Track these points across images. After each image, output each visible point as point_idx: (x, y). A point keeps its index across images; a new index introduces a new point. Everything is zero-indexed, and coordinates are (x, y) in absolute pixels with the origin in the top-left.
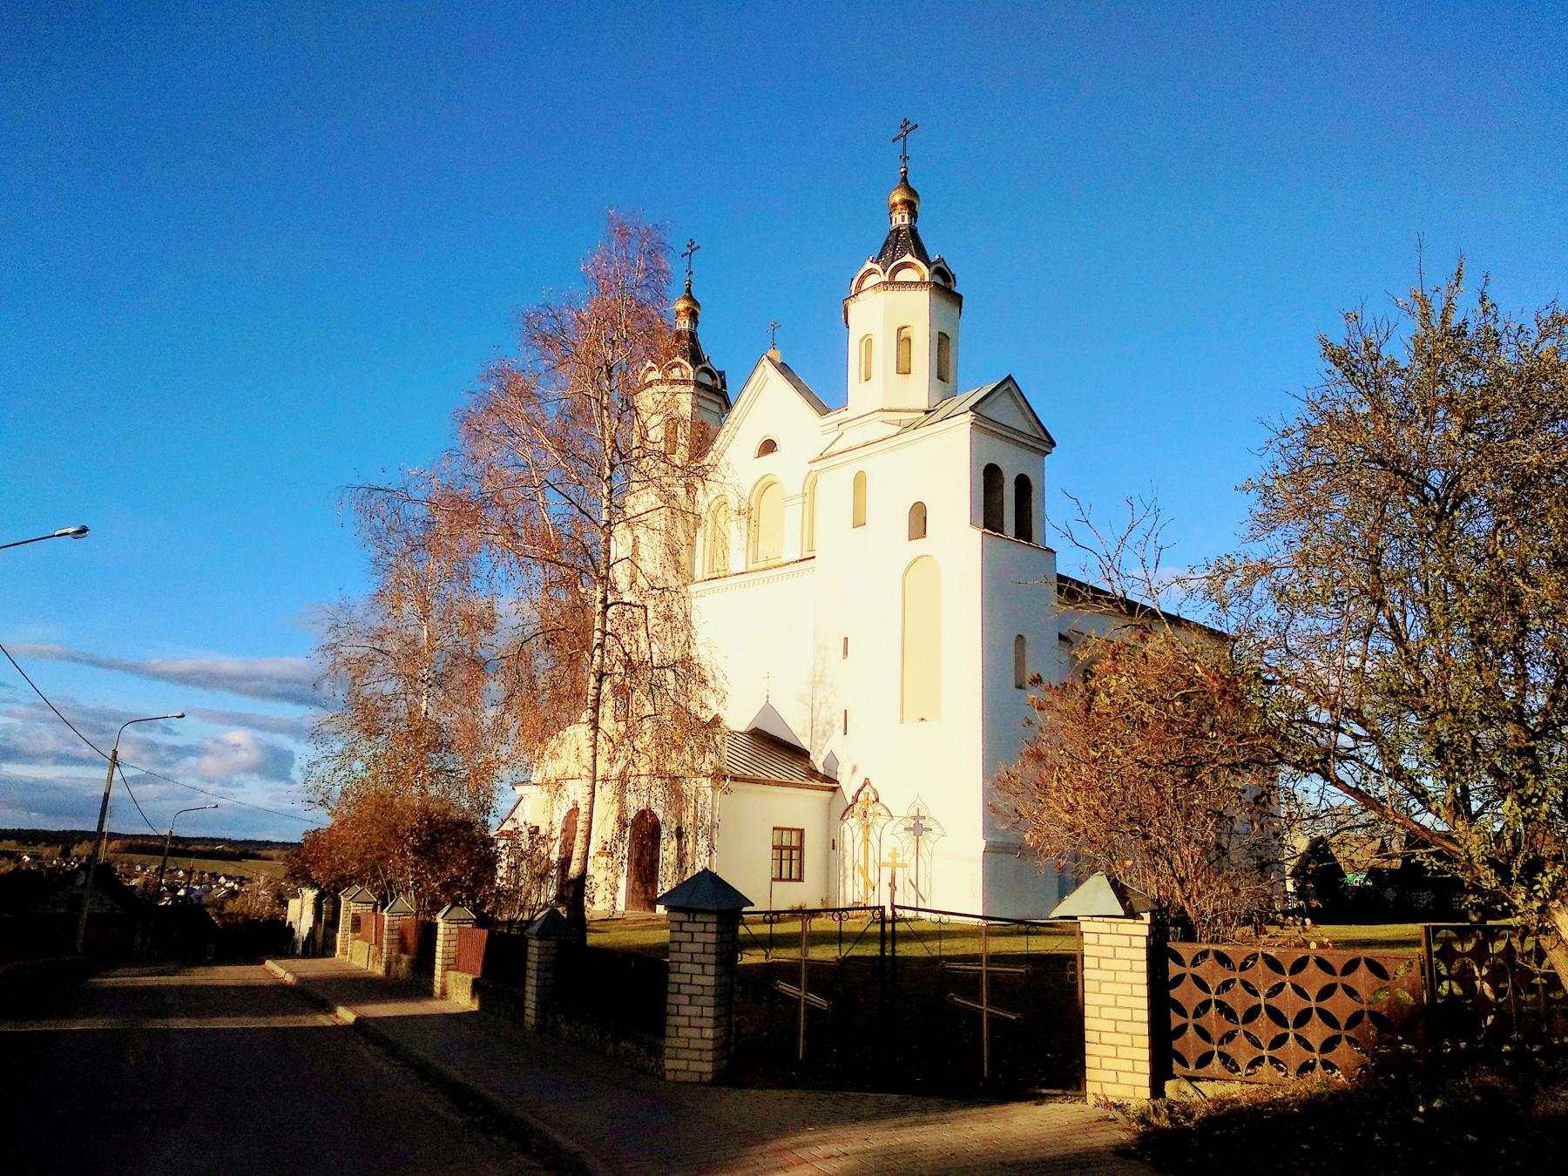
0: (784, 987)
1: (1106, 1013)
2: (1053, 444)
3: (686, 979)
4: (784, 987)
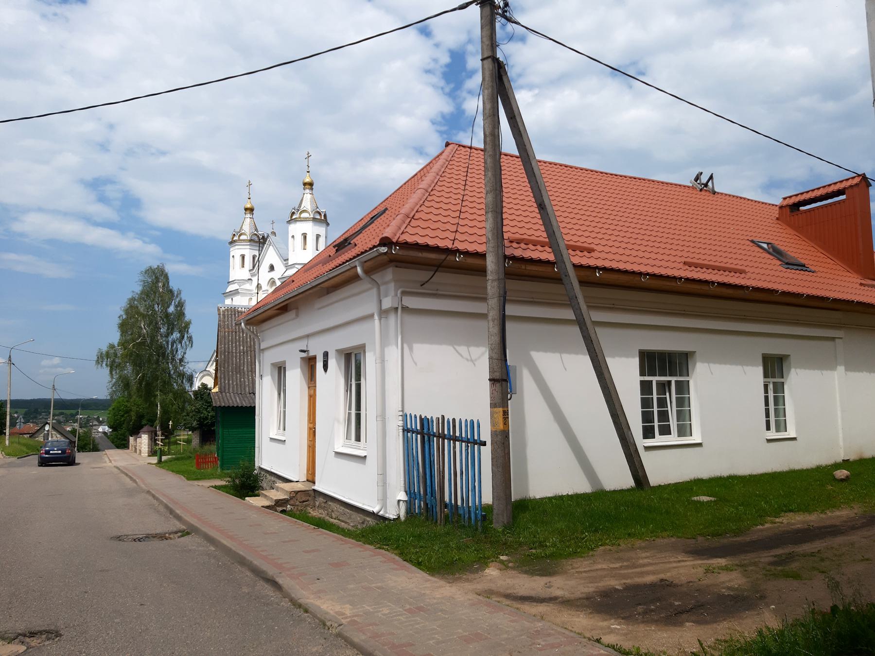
0: (157, 442)
4: (157, 442)
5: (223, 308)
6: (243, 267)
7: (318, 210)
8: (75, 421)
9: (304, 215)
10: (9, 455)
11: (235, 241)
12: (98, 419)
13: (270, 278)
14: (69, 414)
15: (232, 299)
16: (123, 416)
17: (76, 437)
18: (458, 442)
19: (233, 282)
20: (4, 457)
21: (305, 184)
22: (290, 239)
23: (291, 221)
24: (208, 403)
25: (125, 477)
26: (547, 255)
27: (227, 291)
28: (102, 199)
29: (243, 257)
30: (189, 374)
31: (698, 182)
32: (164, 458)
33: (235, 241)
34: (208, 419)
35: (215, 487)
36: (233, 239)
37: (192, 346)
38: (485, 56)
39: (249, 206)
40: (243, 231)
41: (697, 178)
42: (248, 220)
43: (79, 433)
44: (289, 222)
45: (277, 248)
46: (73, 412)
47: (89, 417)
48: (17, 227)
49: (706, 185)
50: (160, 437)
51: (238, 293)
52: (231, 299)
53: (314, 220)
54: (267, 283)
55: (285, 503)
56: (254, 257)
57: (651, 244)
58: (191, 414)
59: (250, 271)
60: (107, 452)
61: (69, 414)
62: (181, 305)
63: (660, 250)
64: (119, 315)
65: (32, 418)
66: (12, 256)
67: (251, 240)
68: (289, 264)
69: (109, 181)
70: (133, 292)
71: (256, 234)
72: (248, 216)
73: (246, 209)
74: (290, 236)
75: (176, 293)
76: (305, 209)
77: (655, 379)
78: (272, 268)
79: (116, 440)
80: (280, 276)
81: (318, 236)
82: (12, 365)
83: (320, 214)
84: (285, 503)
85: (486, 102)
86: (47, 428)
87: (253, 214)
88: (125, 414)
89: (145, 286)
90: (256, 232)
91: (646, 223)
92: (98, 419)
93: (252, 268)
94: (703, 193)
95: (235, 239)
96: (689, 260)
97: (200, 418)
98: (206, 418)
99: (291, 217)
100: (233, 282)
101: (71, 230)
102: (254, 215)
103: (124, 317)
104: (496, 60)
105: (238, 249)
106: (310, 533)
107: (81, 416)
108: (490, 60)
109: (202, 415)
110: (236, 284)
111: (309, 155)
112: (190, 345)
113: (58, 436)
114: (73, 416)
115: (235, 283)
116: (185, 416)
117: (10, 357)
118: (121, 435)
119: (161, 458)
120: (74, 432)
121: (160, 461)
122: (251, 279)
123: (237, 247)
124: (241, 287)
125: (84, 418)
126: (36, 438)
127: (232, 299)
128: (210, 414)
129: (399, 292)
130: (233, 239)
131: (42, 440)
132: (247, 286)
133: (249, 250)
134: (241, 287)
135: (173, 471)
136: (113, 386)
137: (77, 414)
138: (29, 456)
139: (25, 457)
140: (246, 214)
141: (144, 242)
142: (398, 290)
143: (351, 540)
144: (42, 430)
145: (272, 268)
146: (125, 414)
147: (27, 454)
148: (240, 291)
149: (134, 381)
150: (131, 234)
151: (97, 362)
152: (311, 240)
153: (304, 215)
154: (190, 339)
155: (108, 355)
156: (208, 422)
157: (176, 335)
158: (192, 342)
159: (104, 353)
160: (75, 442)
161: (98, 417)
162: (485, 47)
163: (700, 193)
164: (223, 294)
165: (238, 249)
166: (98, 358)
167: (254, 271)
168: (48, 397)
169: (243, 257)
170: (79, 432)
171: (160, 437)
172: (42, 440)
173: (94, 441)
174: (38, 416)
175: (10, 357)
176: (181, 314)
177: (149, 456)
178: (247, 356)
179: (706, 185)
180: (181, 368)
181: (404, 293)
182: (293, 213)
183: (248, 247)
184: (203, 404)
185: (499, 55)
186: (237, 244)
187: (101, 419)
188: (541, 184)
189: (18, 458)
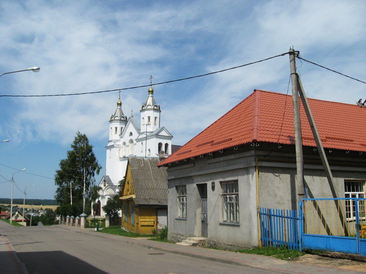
0: (88, 221)
2: (172, 137)
7: (156, 104)
9: (149, 107)
11: (113, 120)
13: (130, 139)
15: (110, 150)
18: (287, 219)
19: (111, 141)
21: (149, 92)
22: (142, 119)
23: (142, 110)
26: (314, 144)
27: (108, 146)
29: (116, 128)
31: (360, 103)
32: (100, 229)
33: (113, 120)
35: (148, 239)
36: (111, 119)
38: (292, 73)
39: (119, 102)
41: (359, 102)
42: (118, 110)
44: (141, 111)
45: (135, 125)
49: (363, 104)
53: (154, 110)
54: (129, 140)
55: (196, 245)
56: (122, 128)
57: (319, 118)
59: (119, 135)
63: (320, 120)
67: (120, 120)
68: (141, 132)
74: (142, 118)
76: (149, 104)
77: (351, 193)
78: (131, 134)
80: (136, 138)
81: (156, 118)
83: (157, 106)
84: (196, 245)
85: (294, 90)
90: (123, 116)
91: (315, 106)
94: (362, 108)
95: (112, 119)
96: (362, 143)
99: (142, 108)
100: (111, 141)
104: (296, 74)
105: (114, 124)
108: (294, 74)
117: (13, 178)
121: (98, 230)
123: (113, 123)
124: (115, 144)
127: (110, 150)
129: (257, 160)
130: (111, 119)
133: (119, 125)
134: (115, 144)
140: (118, 106)
142: (257, 158)
145: (131, 134)
152: (152, 120)
153: (149, 107)
162: (292, 69)
163: (361, 108)
165: (114, 124)
168: (22, 198)
169: (116, 128)
175: (13, 178)
178: (150, 181)
179: (363, 104)
181: (258, 160)
182: (143, 107)
183: (119, 123)
185: (297, 72)
188: (299, 109)
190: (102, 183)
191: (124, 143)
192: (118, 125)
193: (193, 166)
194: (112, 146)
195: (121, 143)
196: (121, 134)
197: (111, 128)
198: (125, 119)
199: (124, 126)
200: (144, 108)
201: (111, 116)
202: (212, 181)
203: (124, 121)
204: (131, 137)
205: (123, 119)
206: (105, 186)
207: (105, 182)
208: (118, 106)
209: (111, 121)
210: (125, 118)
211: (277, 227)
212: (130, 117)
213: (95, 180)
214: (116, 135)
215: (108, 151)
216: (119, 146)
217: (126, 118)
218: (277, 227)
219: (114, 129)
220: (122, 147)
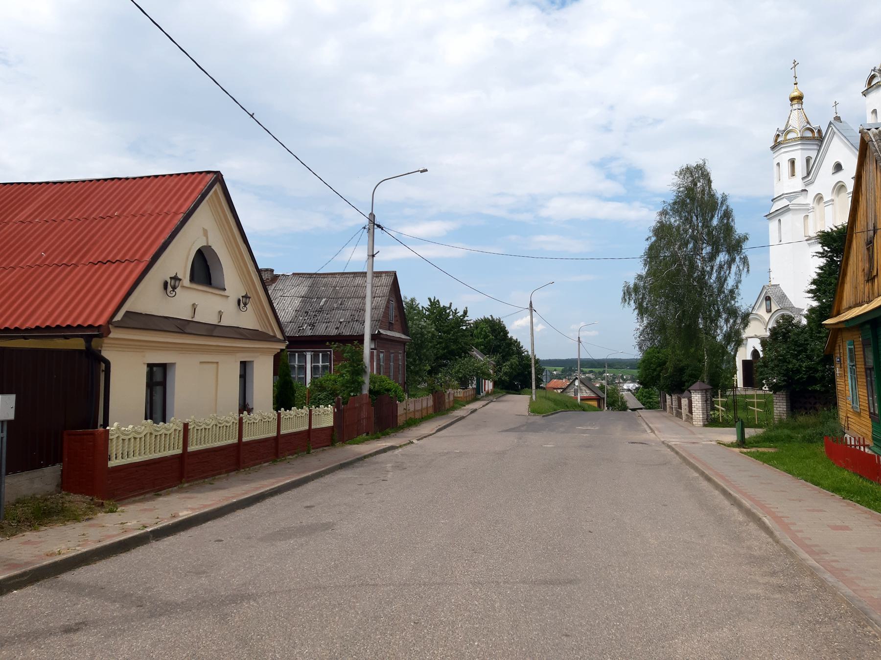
1: (778, 409)
3: (696, 405)
4: (716, 406)
5: (873, 130)
6: (793, 175)
8: (603, 379)
10: (533, 413)
11: (780, 143)
12: (622, 377)
14: (597, 372)
16: (655, 370)
17: (604, 393)
20: (529, 414)
24: (799, 346)
25: (722, 497)
28: (610, 176)
29: (793, 162)
30: (743, 311)
33: (780, 143)
34: (801, 373)
36: (776, 140)
37: (748, 271)
39: (796, 94)
40: (791, 128)
43: (607, 390)
46: (601, 370)
47: (614, 375)
48: (544, 213)
50: (720, 399)
51: (789, 210)
52: (777, 221)
56: (808, 160)
58: (771, 365)
59: (803, 178)
60: (640, 413)
61: (597, 372)
62: (727, 214)
64: (647, 237)
65: (568, 375)
66: (542, 238)
69: (613, 159)
70: (664, 202)
71: (809, 129)
72: (796, 106)
73: (792, 99)
75: (719, 202)
78: (838, 167)
79: (641, 397)
82: (534, 312)
86: (577, 383)
87: (802, 104)
88: (657, 367)
89: (679, 192)
92: (622, 377)
93: (805, 175)
97: (787, 370)
98: (798, 371)
101: (586, 208)
102: (803, 105)
103: (653, 239)
106: (793, 483)
107: (608, 374)
109: (790, 366)
110: (785, 199)
111: (796, 63)
112: (746, 270)
113: (588, 391)
114: (601, 373)
115: (783, 198)
116: (761, 366)
118: (646, 393)
119: (742, 433)
120: (602, 388)
121: (742, 442)
122: (805, 190)
123: (783, 150)
125: (611, 376)
126: (567, 393)
127: (780, 220)
128: (804, 365)
131: (573, 395)
132: (801, 200)
134: (793, 202)
135: (836, 490)
136: (641, 335)
137: (604, 372)
138: (557, 413)
139: (552, 414)
141: (650, 210)
143: (787, 474)
144: (573, 386)
145: (838, 167)
146: (657, 367)
147: (555, 410)
148: (790, 208)
149: (670, 321)
150: (637, 204)
151: (624, 299)
154: (745, 261)
155: (636, 288)
156: (802, 378)
157: (722, 257)
158: (748, 265)
159: (632, 286)
160: (604, 398)
161: (622, 375)
164: (766, 216)
166: (624, 293)
167: (810, 178)
169: (793, 162)
170: (607, 388)
171: (720, 399)
172: (573, 395)
173: (622, 398)
174: (572, 373)
176: (728, 229)
177: (705, 425)
180: (733, 302)
183: (799, 147)
184: (788, 348)
186: (782, 146)
187: (625, 377)
189: (543, 416)
190: (760, 306)
191: (819, 198)
192: (799, 154)
193: (427, 401)
194: (786, 210)
195: (809, 199)
196: (808, 174)
197: (778, 164)
198: (816, 135)
199: (813, 154)
200: (874, 82)
201: (775, 133)
202: (101, 371)
203: (813, 138)
204: (839, 176)
205: (809, 134)
206: (769, 311)
207: (768, 302)
208: (792, 105)
209: (776, 146)
210: (816, 131)
211: (98, 193)
212: (830, 123)
213: (239, 304)
214: (794, 179)
215: (773, 225)
216: (805, 210)
217: (819, 131)
218: (98, 193)
219: (786, 167)
220: (813, 208)
